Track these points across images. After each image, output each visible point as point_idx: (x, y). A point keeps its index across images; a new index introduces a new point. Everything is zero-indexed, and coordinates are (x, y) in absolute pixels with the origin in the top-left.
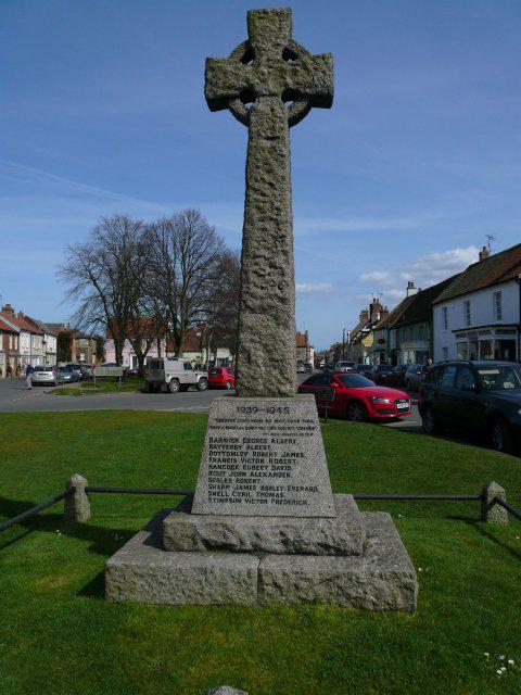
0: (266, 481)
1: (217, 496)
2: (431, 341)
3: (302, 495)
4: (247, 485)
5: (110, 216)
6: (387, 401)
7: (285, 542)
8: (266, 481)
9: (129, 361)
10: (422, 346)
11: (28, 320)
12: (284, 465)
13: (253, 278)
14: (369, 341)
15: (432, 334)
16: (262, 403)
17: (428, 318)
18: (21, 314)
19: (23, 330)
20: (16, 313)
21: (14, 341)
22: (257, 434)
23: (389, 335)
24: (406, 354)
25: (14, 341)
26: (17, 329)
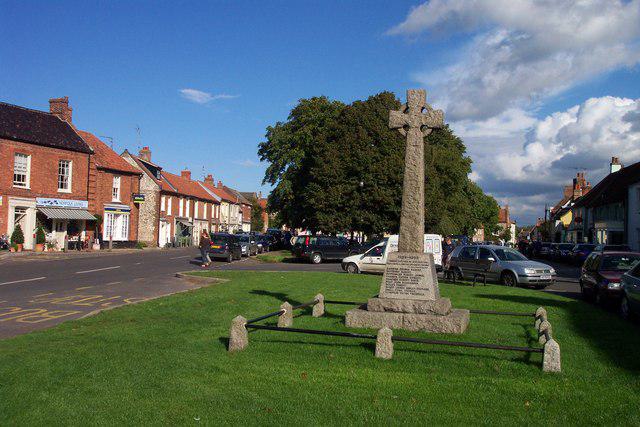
0: (409, 285)
1: (389, 291)
2: (626, 221)
3: (423, 292)
4: (401, 287)
5: (308, 97)
6: (616, 285)
7: (415, 309)
8: (409, 285)
9: (355, 234)
10: (618, 226)
11: (226, 189)
12: (416, 280)
13: (407, 204)
14: (567, 219)
15: (627, 214)
16: (408, 255)
17: (624, 198)
18: (220, 184)
19: (223, 200)
20: (216, 183)
21: (166, 202)
22: (404, 267)
23: (586, 214)
24: (599, 233)
25: (166, 202)
26: (219, 199)
